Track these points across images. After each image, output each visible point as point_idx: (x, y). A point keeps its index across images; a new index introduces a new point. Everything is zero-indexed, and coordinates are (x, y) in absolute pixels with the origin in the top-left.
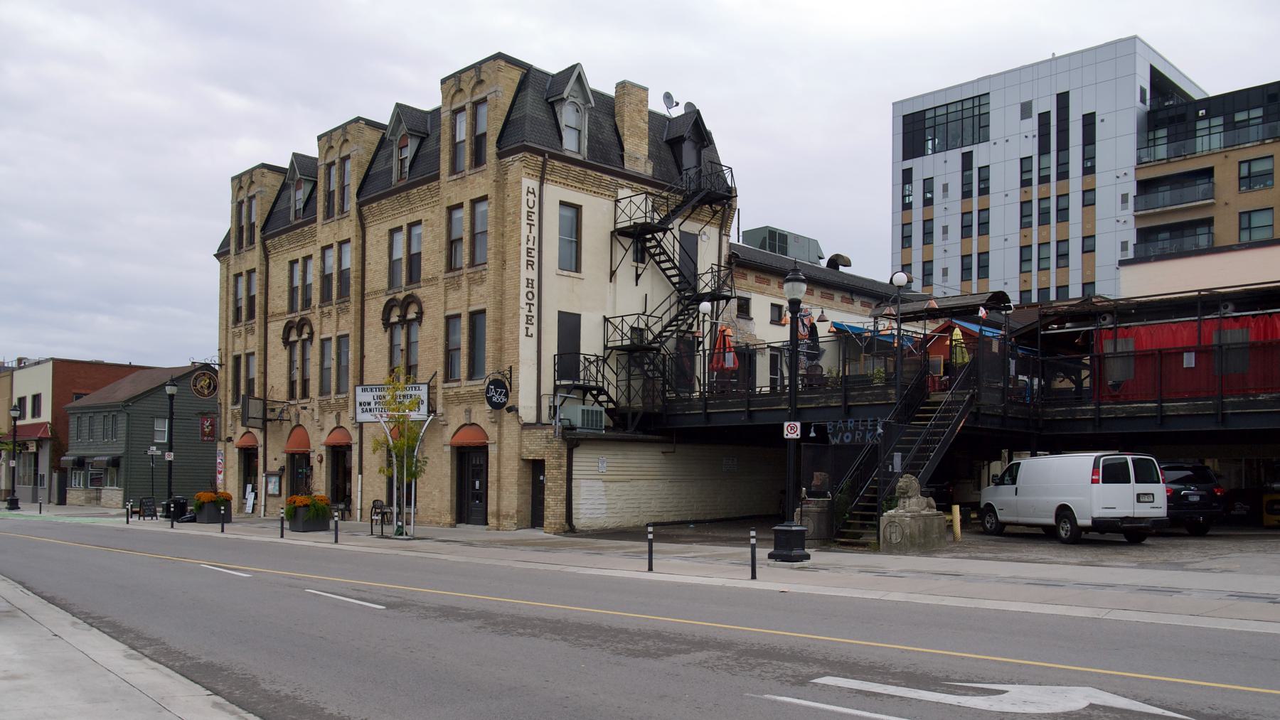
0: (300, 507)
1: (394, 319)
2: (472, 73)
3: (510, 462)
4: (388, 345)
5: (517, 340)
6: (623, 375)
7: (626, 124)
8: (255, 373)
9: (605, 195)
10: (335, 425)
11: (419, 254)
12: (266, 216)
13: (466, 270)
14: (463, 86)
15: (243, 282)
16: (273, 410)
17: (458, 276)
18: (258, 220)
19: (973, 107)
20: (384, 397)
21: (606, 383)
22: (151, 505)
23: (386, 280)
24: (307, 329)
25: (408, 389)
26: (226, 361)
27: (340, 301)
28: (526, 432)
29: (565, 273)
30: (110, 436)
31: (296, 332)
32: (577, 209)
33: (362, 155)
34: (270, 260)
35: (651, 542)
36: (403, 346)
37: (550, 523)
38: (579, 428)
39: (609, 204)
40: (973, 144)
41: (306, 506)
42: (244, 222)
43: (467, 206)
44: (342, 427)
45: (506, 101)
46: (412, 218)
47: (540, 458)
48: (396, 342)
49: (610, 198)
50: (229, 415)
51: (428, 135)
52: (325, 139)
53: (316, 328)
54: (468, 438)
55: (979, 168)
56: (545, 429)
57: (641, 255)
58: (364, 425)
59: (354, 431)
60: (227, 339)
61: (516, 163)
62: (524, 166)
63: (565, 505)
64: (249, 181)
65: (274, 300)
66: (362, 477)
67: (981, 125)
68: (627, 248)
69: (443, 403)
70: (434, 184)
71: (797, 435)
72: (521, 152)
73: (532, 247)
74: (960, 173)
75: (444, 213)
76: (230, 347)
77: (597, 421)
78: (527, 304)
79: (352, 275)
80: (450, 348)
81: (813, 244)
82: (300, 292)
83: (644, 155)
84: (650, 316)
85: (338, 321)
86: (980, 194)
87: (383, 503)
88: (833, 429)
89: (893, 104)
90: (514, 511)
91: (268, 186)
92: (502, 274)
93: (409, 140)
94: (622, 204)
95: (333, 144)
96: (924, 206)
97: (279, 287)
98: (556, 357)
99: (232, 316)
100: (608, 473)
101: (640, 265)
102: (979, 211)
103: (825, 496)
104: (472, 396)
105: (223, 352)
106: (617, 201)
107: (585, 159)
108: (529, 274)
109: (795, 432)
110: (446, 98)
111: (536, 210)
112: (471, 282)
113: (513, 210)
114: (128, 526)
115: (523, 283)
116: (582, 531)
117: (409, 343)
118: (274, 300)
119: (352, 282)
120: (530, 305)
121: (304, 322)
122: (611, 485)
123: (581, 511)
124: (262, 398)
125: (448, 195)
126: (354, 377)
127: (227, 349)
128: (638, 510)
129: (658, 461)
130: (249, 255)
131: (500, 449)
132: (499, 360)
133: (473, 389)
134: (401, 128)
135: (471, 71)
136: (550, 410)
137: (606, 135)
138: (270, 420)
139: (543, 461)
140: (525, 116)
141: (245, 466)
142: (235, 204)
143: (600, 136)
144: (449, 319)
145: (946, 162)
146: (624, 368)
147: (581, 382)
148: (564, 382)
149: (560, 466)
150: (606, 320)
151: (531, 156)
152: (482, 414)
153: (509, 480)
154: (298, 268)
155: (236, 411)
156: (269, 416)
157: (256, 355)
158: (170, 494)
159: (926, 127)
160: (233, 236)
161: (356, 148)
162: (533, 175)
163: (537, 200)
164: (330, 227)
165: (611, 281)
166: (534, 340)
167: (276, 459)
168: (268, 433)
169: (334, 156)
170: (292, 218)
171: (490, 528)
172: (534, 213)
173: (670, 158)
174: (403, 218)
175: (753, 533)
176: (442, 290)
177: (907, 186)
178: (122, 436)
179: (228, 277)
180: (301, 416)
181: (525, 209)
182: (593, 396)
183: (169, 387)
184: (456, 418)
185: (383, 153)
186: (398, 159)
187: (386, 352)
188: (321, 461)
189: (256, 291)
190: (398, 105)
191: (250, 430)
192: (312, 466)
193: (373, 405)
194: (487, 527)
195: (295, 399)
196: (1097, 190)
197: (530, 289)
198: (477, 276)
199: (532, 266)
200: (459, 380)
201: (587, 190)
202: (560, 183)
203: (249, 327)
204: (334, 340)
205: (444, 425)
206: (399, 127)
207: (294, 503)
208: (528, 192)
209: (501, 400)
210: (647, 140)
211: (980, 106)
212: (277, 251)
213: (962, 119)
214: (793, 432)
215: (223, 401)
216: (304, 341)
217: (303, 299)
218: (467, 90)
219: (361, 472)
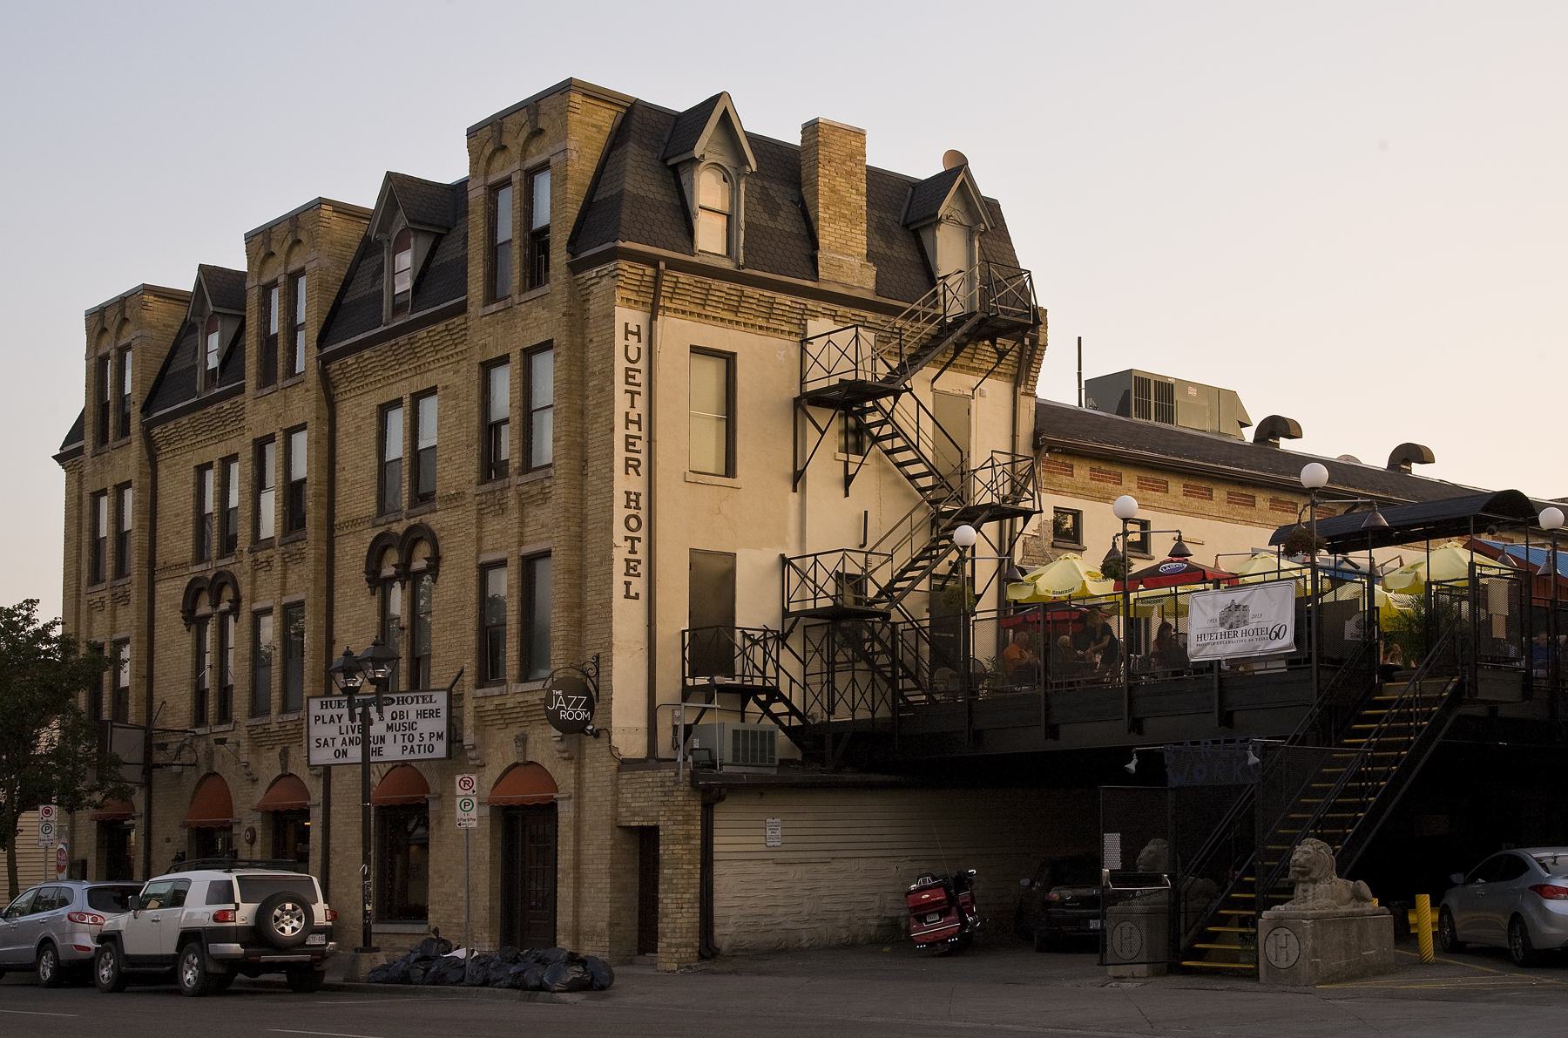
1: (388, 571)
4: (377, 619)
6: (815, 665)
9: (782, 331)
12: (151, 383)
13: (515, 479)
16: (164, 747)
17: (501, 490)
21: (783, 677)
23: (373, 498)
24: (228, 593)
25: (409, 700)
32: (729, 360)
34: (160, 466)
37: (670, 945)
39: (789, 347)
46: (419, 384)
47: (651, 824)
52: (261, 241)
53: (245, 591)
54: (521, 794)
56: (659, 769)
57: (857, 439)
58: (334, 771)
60: (78, 614)
61: (604, 281)
63: (698, 910)
65: (167, 539)
68: (823, 430)
69: (475, 726)
70: (458, 320)
75: (475, 376)
77: (763, 751)
78: (626, 538)
81: (1225, 400)
84: (870, 552)
85: (284, 576)
90: (604, 924)
91: (155, 327)
95: (275, 248)
98: (687, 633)
100: (786, 847)
101: (853, 458)
104: (526, 713)
106: (804, 341)
111: (642, 365)
118: (167, 539)
126: (314, 681)
130: (118, 457)
131: (579, 808)
133: (528, 698)
138: (158, 766)
139: (656, 829)
142: (93, 361)
146: (817, 650)
147: (738, 681)
149: (688, 837)
150: (785, 561)
152: (545, 746)
153: (594, 867)
154: (397, 421)
156: (159, 758)
160: (89, 420)
161: (315, 254)
163: (643, 346)
164: (269, 403)
166: (641, 604)
167: (168, 840)
169: (276, 271)
172: (640, 371)
176: (472, 516)
179: (80, 498)
182: (757, 701)
184: (500, 754)
185: (369, 265)
190: (389, 176)
199: (635, 468)
205: (478, 766)
206: (394, 215)
208: (627, 332)
209: (579, 715)
212: (173, 447)
218: (515, 149)
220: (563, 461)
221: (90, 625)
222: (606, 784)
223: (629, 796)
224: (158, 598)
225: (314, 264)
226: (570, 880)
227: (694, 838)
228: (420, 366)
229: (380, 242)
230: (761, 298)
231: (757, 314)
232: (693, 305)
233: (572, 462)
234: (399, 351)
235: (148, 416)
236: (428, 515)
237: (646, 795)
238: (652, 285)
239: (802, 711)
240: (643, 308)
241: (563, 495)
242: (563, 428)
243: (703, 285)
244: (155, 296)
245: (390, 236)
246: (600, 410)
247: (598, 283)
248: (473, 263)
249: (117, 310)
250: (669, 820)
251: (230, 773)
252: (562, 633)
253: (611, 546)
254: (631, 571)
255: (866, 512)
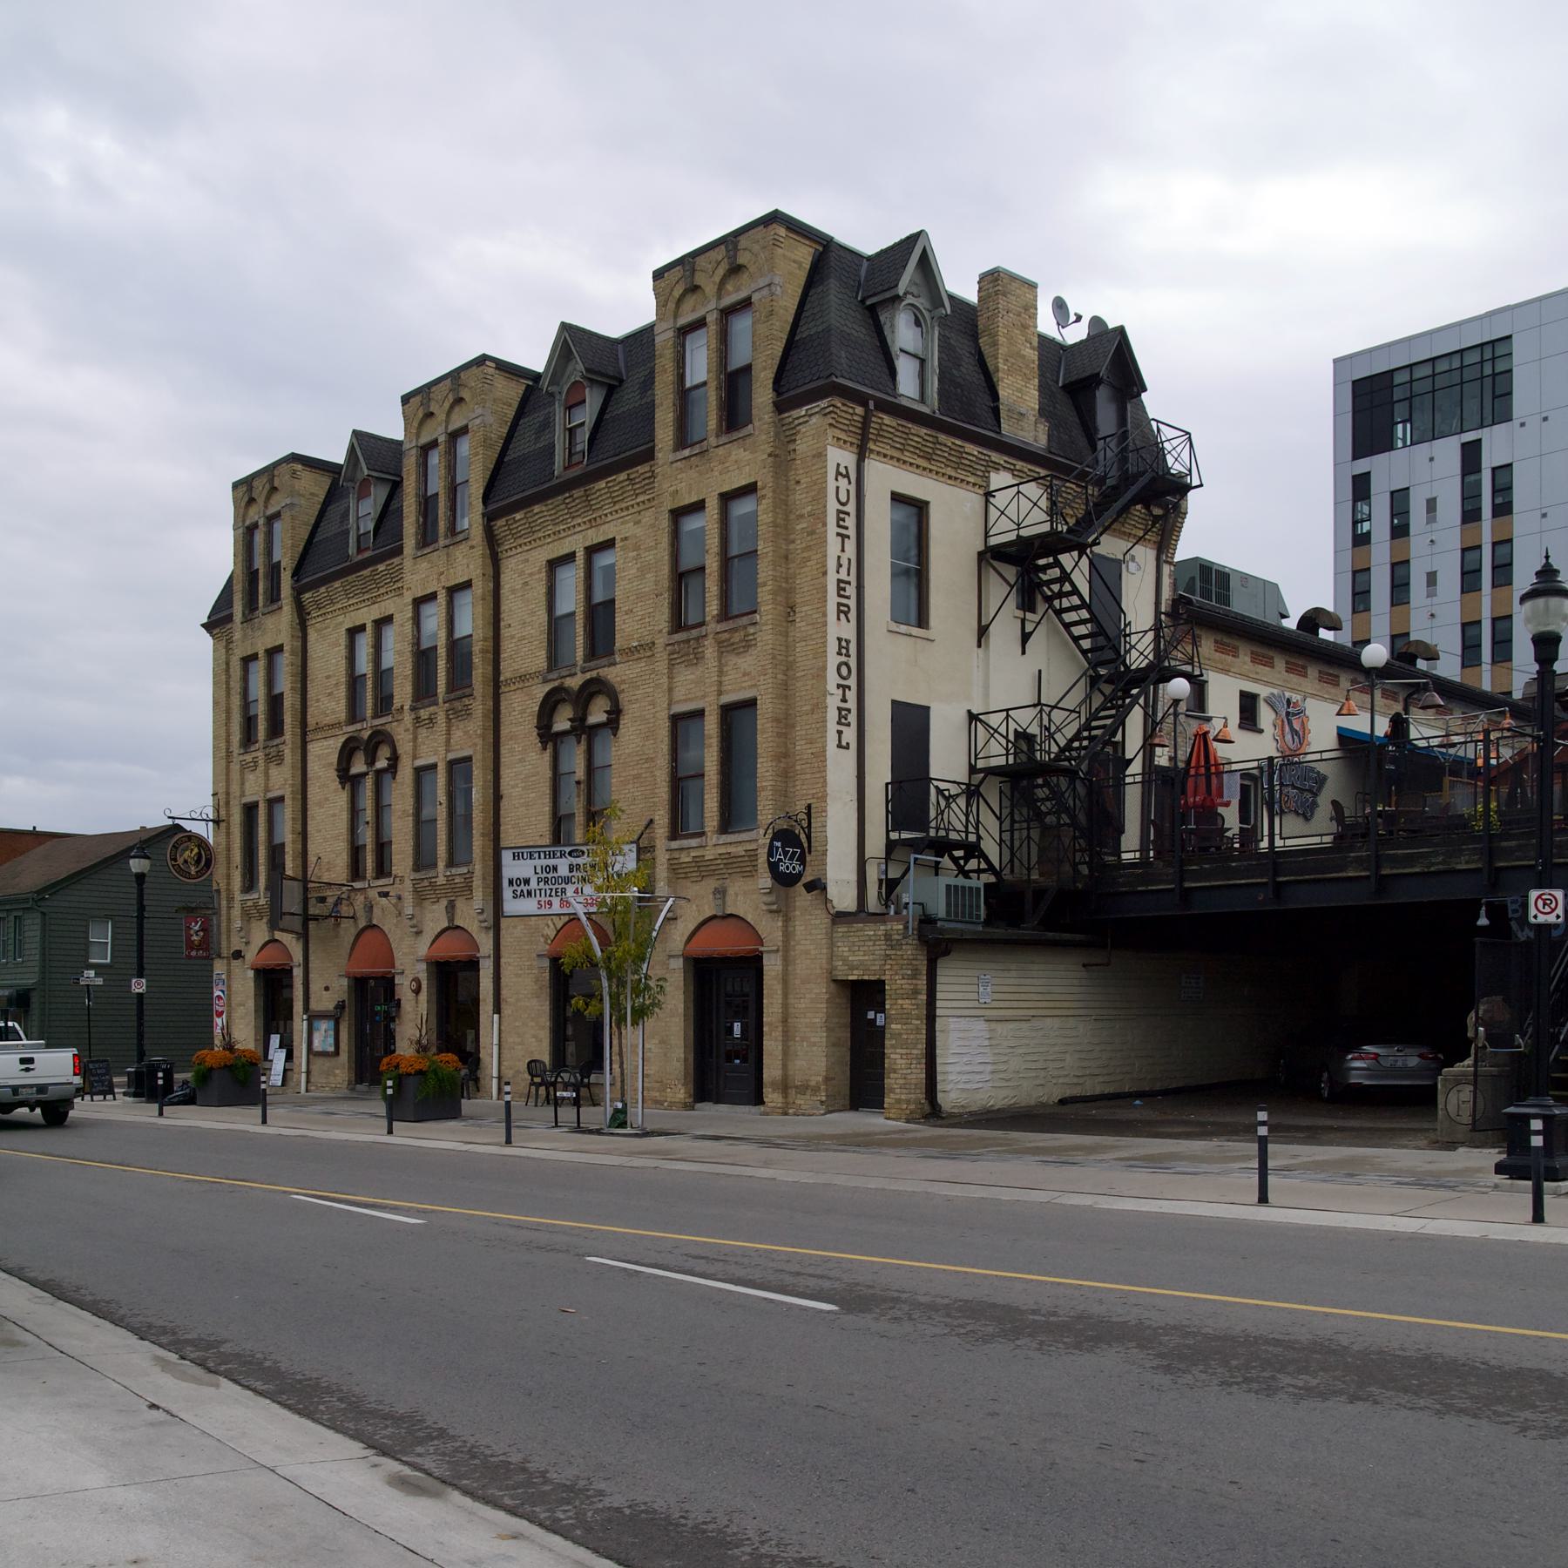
0: (409, 1075)
1: (562, 723)
2: (720, 253)
3: (808, 986)
4: (548, 774)
5: (821, 755)
7: (1002, 350)
8: (287, 834)
9: (968, 483)
10: (446, 925)
11: (610, 604)
12: (301, 548)
13: (713, 627)
14: (700, 279)
15: (258, 671)
17: (697, 639)
18: (285, 556)
19: (1482, 362)
20: (555, 869)
22: (104, 1075)
23: (543, 654)
24: (384, 753)
26: (228, 815)
27: (452, 696)
28: (842, 929)
29: (903, 628)
30: (11, 953)
31: (363, 758)
32: (919, 508)
33: (491, 425)
35: (1263, 1142)
36: (580, 774)
37: (898, 1101)
38: (940, 920)
39: (973, 500)
40: (1482, 426)
41: (420, 1073)
42: (259, 563)
43: (712, 506)
44: (458, 927)
45: (788, 303)
46: (595, 536)
47: (872, 978)
48: (563, 768)
49: (976, 489)
50: (236, 912)
51: (621, 381)
52: (418, 402)
53: (404, 748)
55: (1494, 469)
57: (1029, 594)
59: (483, 935)
61: (814, 420)
62: (831, 425)
63: (924, 1066)
64: (268, 487)
65: (318, 701)
66: (500, 1017)
67: (1497, 394)
71: (1558, 917)
72: (826, 397)
73: (845, 578)
74: (1459, 479)
75: (665, 522)
76: (235, 788)
77: (971, 906)
79: (476, 648)
80: (680, 775)
81: (1269, 590)
82: (369, 684)
83: (1033, 409)
85: (449, 733)
86: (1495, 515)
87: (545, 1065)
88: (1520, 910)
89: (1335, 361)
91: (303, 496)
92: (787, 632)
93: (587, 390)
94: (1000, 500)
95: (434, 408)
96: (1393, 538)
97: (328, 677)
99: (238, 733)
100: (995, 1004)
101: (1029, 616)
102: (1494, 544)
103: (1511, 1044)
105: (221, 799)
106: (988, 495)
107: (934, 412)
108: (840, 629)
109: (1553, 910)
110: (665, 306)
111: (851, 508)
112: (724, 648)
113: (809, 508)
114: (1537, 1234)
115: (832, 647)
116: (951, 1115)
117: (590, 769)
118: (318, 701)
119: (476, 660)
120: (845, 688)
121: (380, 738)
122: (999, 1027)
123: (951, 1077)
124: (300, 877)
125: (672, 489)
126: (483, 835)
127: (228, 794)
128: (1042, 1073)
129: (1075, 982)
130: (270, 622)
131: (786, 961)
132: (783, 794)
133: (731, 849)
134: (570, 368)
135: (717, 250)
136: (880, 888)
137: (965, 371)
138: (316, 918)
140: (828, 330)
141: (266, 1003)
142: (241, 531)
143: (955, 372)
144: (677, 720)
145: (1431, 459)
147: (932, 833)
148: (905, 835)
149: (916, 992)
150: (973, 717)
151: (844, 405)
153: (808, 1020)
154: (364, 643)
155: (250, 903)
156: (314, 910)
157: (288, 801)
158: (141, 1055)
159: (1395, 399)
160: (238, 588)
161: (479, 411)
162: (845, 442)
163: (853, 489)
165: (979, 646)
166: (852, 752)
167: (327, 989)
168: (310, 938)
169: (435, 431)
170: (352, 550)
171: (768, 1110)
172: (848, 514)
173: (1073, 418)
174: (575, 537)
175: (1262, 1116)
176: (662, 666)
177: (1359, 503)
178: (33, 952)
180: (375, 910)
181: (832, 507)
182: (955, 860)
183: (137, 860)
184: (697, 904)
186: (565, 429)
187: (546, 789)
188: (417, 991)
189: (285, 684)
191: (278, 935)
192: (399, 1000)
193: (533, 884)
194: (762, 1108)
195: (364, 878)
196: (1514, 540)
197: (844, 659)
198: (737, 637)
199: (846, 614)
200: (702, 834)
201: (937, 473)
202: (892, 458)
203: (273, 751)
204: (442, 768)
207: (397, 1067)
208: (838, 473)
210: (1037, 380)
211: (1493, 359)
213: (1462, 383)
214: (1547, 909)
215: (223, 886)
216: (379, 773)
217: (375, 697)
218: (710, 288)
219: (497, 1009)
220: (770, 606)
221: (243, 784)
222: (819, 937)
223: (847, 949)
224: (310, 758)
225: (478, 421)
226: (778, 1034)
227: (921, 994)
228: (595, 519)
229: (552, 395)
230: (953, 447)
231: (948, 463)
232: (893, 450)
233: (778, 607)
234: (573, 504)
235: (297, 581)
236: (606, 669)
237: (866, 948)
238: (860, 425)
239: (998, 868)
240: (851, 449)
241: (770, 642)
242: (770, 573)
243: (904, 429)
244: (303, 465)
245: (562, 388)
246: (810, 553)
247: (807, 421)
248: (661, 408)
249: (245, 489)
250: (896, 974)
251: (388, 924)
252: (771, 783)
253: (825, 693)
254: (843, 720)
255: (1040, 671)
